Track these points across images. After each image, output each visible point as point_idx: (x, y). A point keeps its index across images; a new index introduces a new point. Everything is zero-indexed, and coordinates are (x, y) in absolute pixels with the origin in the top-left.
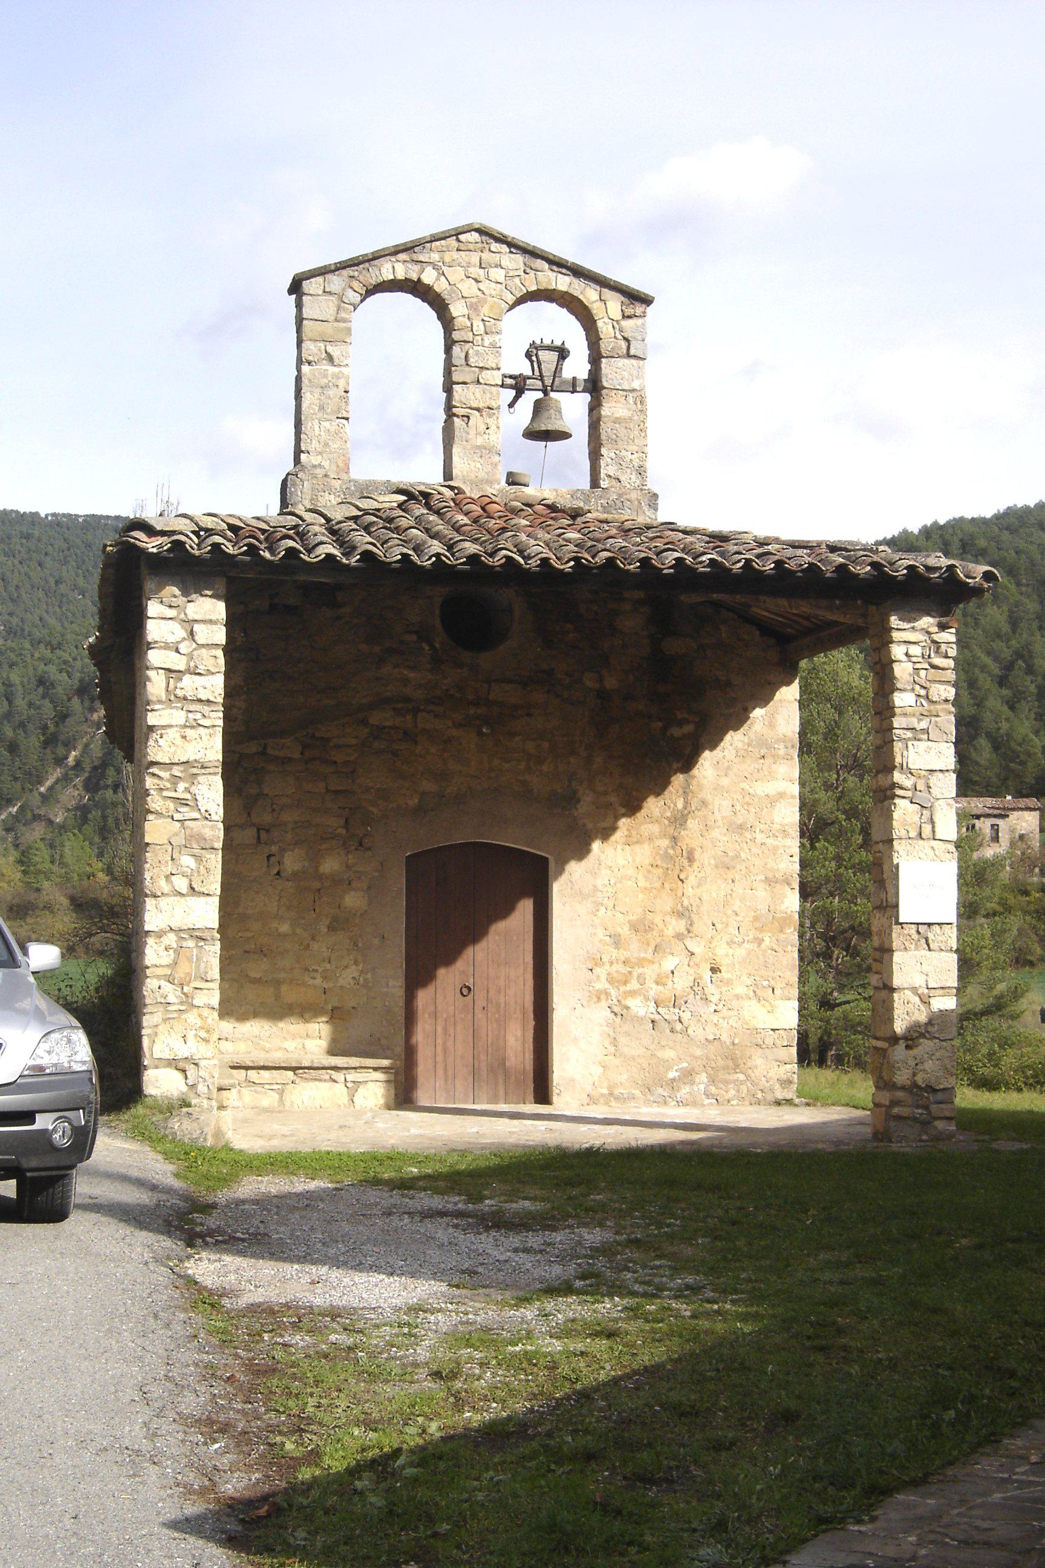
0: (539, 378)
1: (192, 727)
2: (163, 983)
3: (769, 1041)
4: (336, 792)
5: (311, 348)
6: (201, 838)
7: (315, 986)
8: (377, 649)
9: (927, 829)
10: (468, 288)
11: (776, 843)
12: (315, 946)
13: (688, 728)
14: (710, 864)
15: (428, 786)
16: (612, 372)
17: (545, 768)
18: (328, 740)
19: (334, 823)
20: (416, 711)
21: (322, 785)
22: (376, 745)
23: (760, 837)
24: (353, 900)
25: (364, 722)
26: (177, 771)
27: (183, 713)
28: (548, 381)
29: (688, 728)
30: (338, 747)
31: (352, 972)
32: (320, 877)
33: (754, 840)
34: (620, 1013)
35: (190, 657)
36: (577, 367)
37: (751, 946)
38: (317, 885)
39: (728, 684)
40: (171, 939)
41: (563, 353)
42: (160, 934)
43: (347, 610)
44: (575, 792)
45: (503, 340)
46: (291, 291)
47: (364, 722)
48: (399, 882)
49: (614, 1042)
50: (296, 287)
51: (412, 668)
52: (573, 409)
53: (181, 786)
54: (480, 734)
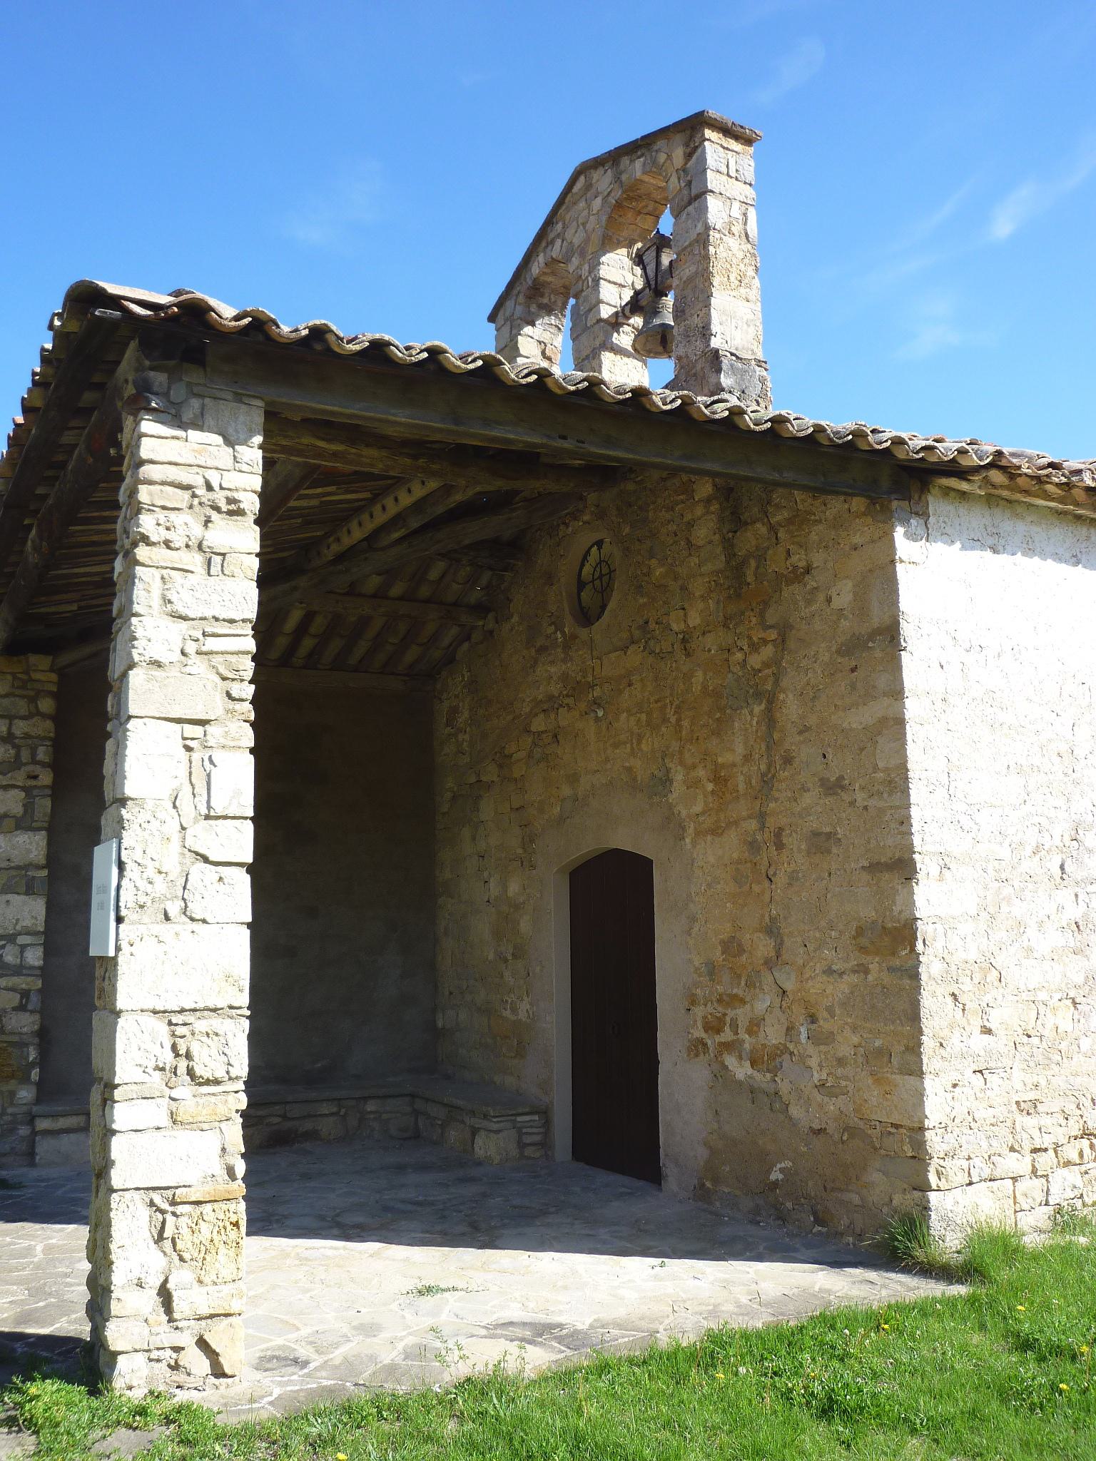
11: (881, 804)
14: (800, 851)
23: (860, 797)
33: (852, 803)
37: (854, 979)
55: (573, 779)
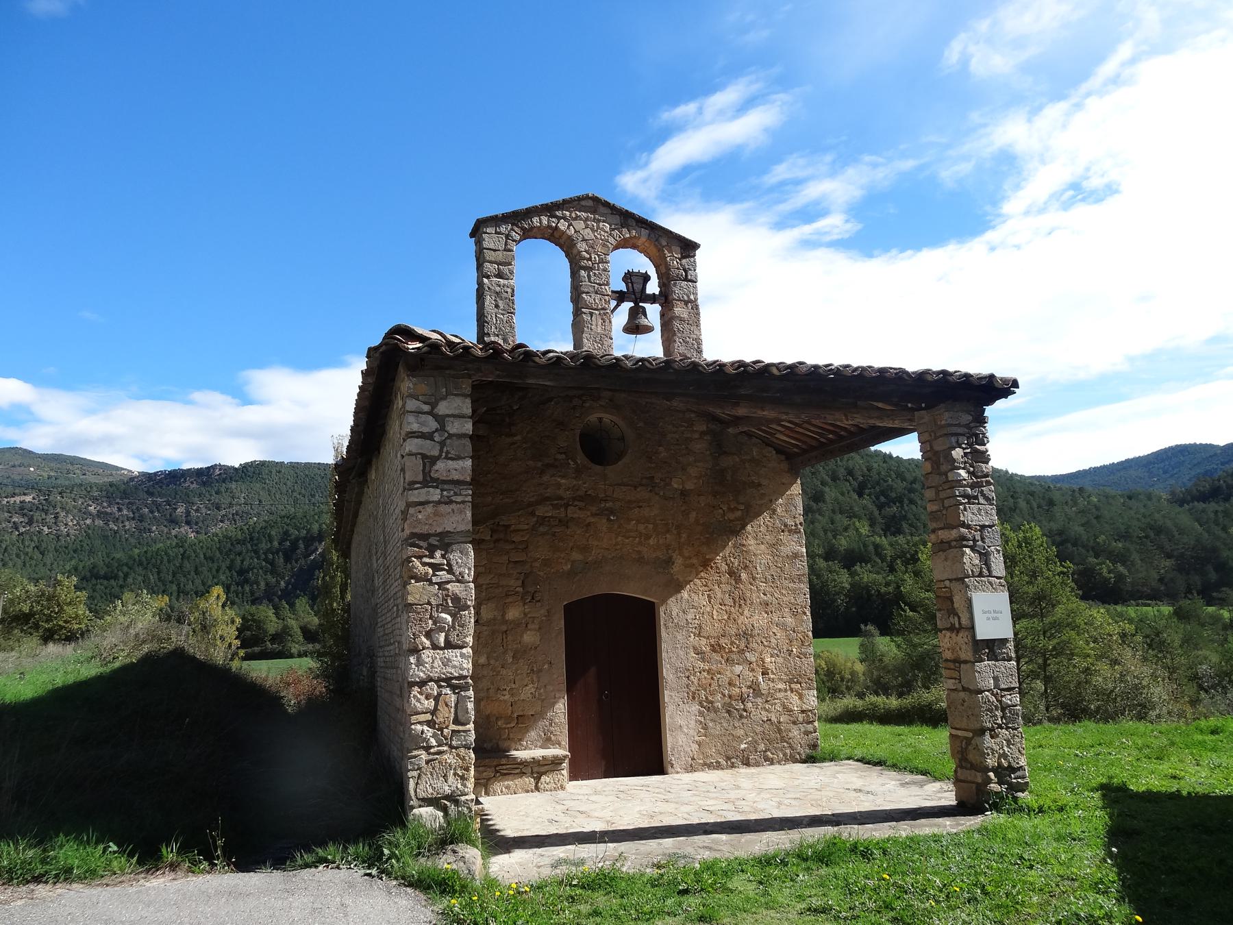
0: (634, 290)
1: (446, 503)
2: (426, 728)
3: (801, 719)
4: (516, 562)
5: (490, 268)
6: (456, 599)
7: (505, 701)
8: (539, 464)
9: (985, 571)
10: (588, 234)
12: (504, 672)
13: (739, 514)
15: (576, 556)
16: (679, 289)
17: (651, 542)
18: (509, 526)
19: (514, 583)
20: (567, 506)
21: (506, 558)
22: (542, 529)
24: (529, 638)
25: (533, 514)
26: (433, 541)
27: (438, 491)
28: (638, 295)
29: (739, 514)
30: (515, 531)
31: (530, 689)
32: (505, 622)
34: (708, 706)
35: (442, 444)
36: (653, 287)
38: (504, 628)
39: (760, 485)
40: (433, 688)
41: (646, 278)
42: (422, 684)
43: (518, 438)
44: (671, 558)
45: (610, 267)
46: (472, 235)
47: (533, 514)
48: (560, 624)
49: (705, 727)
50: (477, 231)
51: (563, 477)
52: (653, 312)
53: (438, 554)
54: (609, 520)
55: (585, 549)
